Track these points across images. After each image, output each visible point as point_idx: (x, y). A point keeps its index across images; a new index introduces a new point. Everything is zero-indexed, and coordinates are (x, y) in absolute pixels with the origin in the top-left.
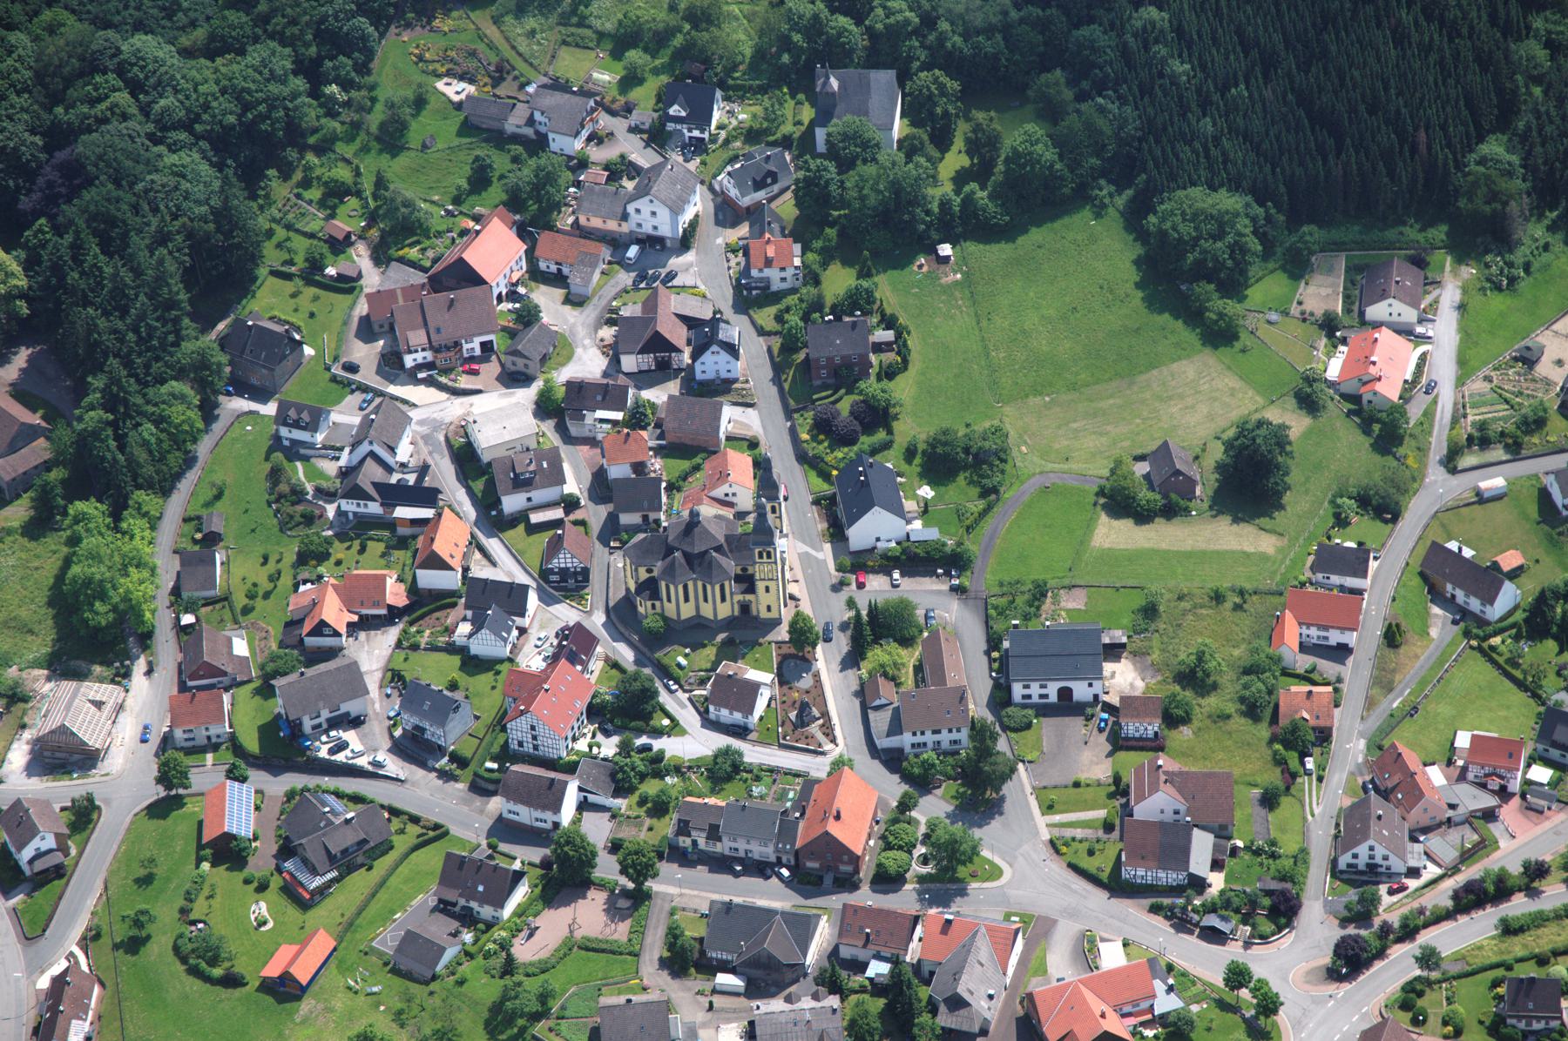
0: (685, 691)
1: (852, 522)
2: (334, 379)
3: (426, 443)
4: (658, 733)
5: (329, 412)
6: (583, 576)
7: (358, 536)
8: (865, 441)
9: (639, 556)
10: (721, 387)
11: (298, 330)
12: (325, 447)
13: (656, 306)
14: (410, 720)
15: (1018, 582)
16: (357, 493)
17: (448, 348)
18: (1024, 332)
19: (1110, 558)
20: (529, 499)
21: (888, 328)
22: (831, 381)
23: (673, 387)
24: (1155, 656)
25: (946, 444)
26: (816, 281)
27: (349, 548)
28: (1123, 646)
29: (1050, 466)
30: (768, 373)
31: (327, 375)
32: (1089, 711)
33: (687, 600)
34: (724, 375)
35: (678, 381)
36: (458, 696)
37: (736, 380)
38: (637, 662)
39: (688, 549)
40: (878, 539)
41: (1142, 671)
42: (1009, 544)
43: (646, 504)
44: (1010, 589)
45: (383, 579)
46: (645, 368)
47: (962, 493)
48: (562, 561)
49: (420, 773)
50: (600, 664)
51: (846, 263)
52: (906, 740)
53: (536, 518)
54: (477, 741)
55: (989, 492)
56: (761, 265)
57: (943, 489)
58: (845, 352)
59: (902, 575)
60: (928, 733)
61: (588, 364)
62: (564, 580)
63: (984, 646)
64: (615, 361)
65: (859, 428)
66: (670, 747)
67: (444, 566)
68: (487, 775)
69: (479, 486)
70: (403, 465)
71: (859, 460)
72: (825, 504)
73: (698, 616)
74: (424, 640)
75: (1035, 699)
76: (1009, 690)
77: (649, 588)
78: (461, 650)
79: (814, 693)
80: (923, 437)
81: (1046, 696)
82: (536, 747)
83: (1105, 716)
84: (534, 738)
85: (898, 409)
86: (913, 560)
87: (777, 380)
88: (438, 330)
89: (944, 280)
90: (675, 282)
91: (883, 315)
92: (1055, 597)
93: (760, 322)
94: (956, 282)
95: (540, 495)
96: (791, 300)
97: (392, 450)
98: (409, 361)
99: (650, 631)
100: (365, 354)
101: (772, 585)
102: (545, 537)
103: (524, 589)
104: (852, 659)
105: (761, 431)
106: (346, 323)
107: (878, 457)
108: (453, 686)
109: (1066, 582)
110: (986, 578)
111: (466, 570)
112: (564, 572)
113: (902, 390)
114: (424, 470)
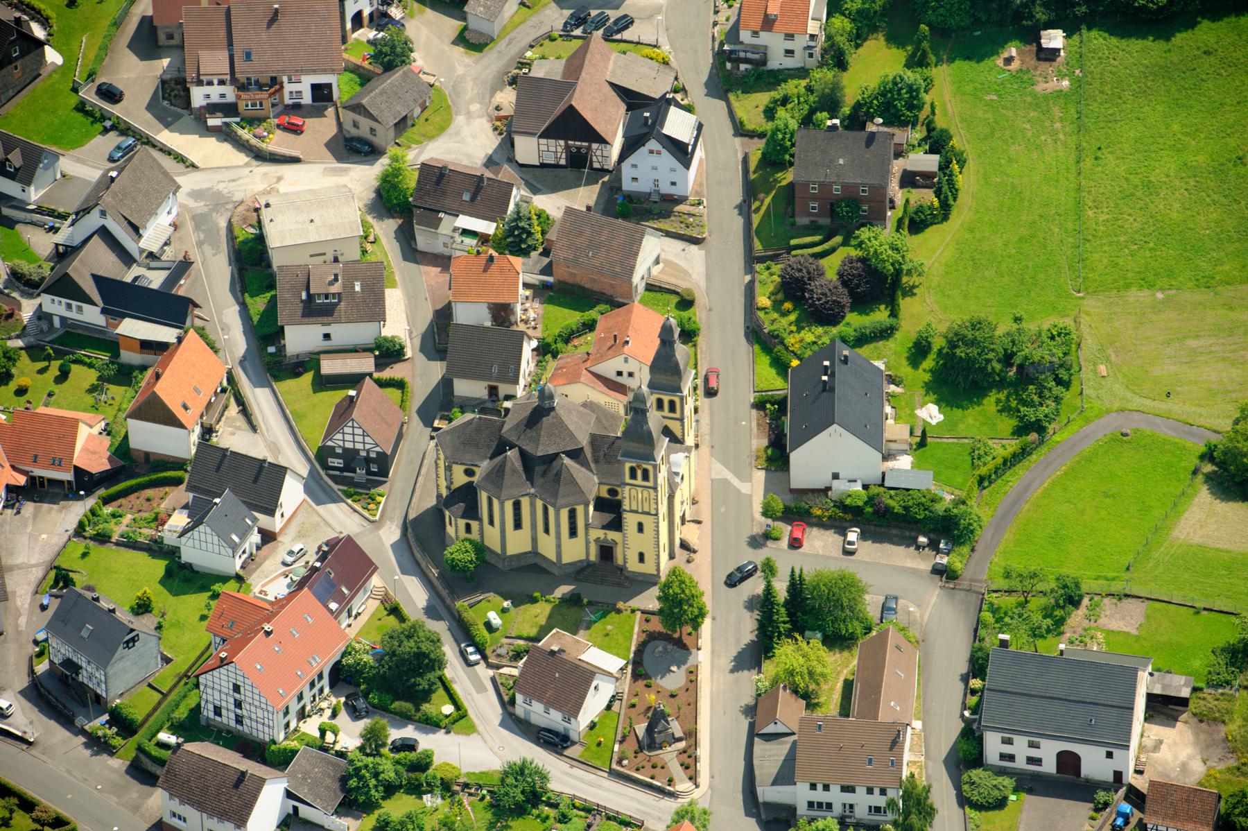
0: (490, 666)
1: (793, 449)
2: (81, 108)
3: (197, 227)
4: (431, 724)
5: (56, 156)
6: (380, 466)
7: (59, 354)
8: (854, 321)
9: (461, 446)
10: (652, 208)
11: (45, 22)
12: (40, 210)
13: (580, 68)
14: (60, 650)
15: (1034, 575)
16: (65, 287)
17: (260, 86)
18: (1148, 185)
19: (1200, 561)
20: (327, 336)
21: (932, 151)
22: (825, 221)
23: (585, 196)
24: (1234, 727)
25: (973, 343)
26: (841, 64)
27: (42, 371)
28: (1184, 702)
29: (1137, 402)
30: (736, 194)
31: (74, 100)
32: (1101, 796)
33: (518, 525)
34: (666, 189)
35: (596, 188)
36: (144, 624)
37: (681, 200)
38: (431, 612)
39: (528, 448)
40: (836, 476)
41: (1205, 748)
42: (1041, 518)
43: (495, 369)
44: (1021, 585)
45: (73, 425)
46: (550, 160)
47: (987, 424)
48: (347, 439)
49: (59, 733)
50: (374, 605)
51: (894, 39)
52: (799, 794)
53: (329, 366)
54: (158, 696)
55: (1031, 428)
56: (757, 23)
57: (958, 413)
58: (851, 179)
59: (863, 536)
60: (835, 789)
61: (466, 143)
62: (348, 468)
63: (964, 667)
64: (508, 144)
65: (846, 300)
66: (446, 751)
67: (169, 419)
68: (156, 752)
69: (258, 304)
70: (151, 255)
71: (829, 351)
72: (772, 409)
73: (535, 552)
74: (117, 530)
75: (1020, 763)
76: (980, 741)
77: (464, 499)
78: (171, 553)
79: (683, 698)
80: (942, 328)
81: (1038, 761)
82: (239, 720)
83: (1127, 808)
84: (238, 704)
85: (914, 280)
86: (885, 518)
87: (745, 209)
88: (248, 56)
89: (1040, 87)
90: (626, 35)
91: (930, 128)
92: (1093, 607)
93: (741, 114)
94: (1059, 93)
95: (343, 333)
96: (793, 87)
97: (136, 229)
98: (198, 96)
99: (454, 566)
100: (138, 77)
101: (646, 520)
102: (335, 397)
103: (279, 472)
104: (756, 654)
105: (702, 283)
106: (118, 24)
107: (864, 351)
108: (143, 607)
109: (1117, 587)
110: (990, 561)
111: (208, 431)
112: (350, 456)
113: (928, 253)
114: (183, 266)
